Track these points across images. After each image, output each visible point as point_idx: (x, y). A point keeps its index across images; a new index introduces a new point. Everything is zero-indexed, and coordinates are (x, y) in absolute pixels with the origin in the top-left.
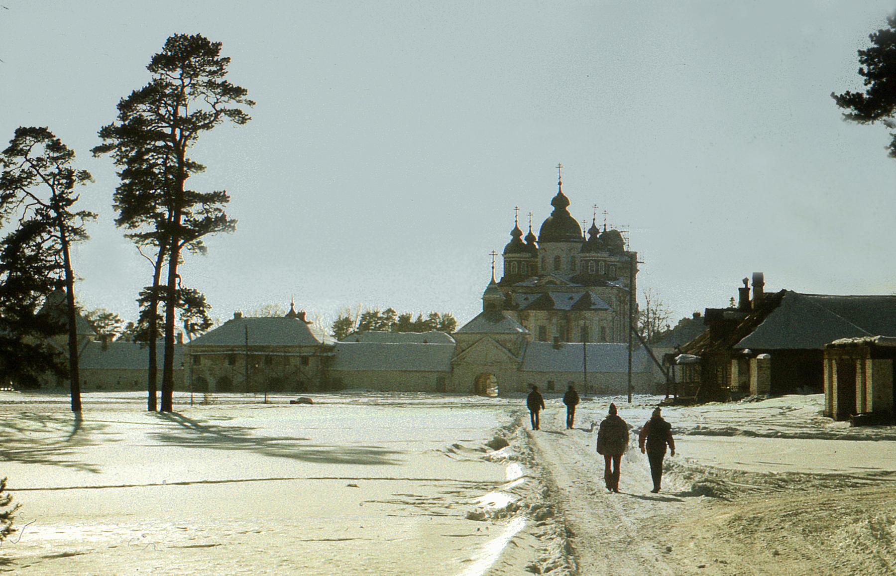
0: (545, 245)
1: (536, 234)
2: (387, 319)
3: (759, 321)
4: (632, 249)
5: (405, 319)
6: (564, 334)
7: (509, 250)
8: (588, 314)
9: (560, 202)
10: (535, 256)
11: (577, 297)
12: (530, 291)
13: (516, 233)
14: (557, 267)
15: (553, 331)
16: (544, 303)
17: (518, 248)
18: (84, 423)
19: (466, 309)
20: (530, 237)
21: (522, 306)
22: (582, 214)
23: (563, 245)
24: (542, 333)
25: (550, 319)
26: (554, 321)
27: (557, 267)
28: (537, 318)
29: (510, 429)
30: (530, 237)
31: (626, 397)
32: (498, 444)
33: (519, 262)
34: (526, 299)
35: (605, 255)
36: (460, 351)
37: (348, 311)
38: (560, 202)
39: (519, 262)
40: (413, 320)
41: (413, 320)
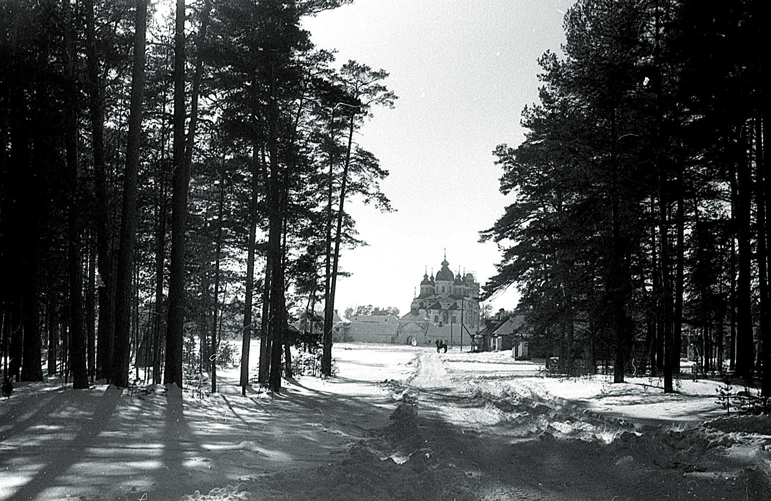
0: (438, 281)
1: (435, 276)
2: (369, 309)
3: (502, 324)
4: (478, 282)
6: (445, 320)
7: (422, 283)
8: (455, 311)
9: (445, 264)
10: (434, 286)
11: (451, 304)
12: (431, 301)
13: (426, 276)
14: (443, 291)
16: (437, 306)
17: (427, 282)
18: (337, 365)
19: (405, 309)
20: (432, 278)
21: (428, 308)
22: (454, 268)
23: (447, 282)
25: (439, 313)
26: (441, 314)
27: (443, 291)
28: (433, 313)
29: (415, 360)
30: (432, 278)
31: (460, 347)
32: (410, 363)
33: (427, 289)
35: (464, 286)
36: (401, 327)
37: (352, 305)
38: (445, 264)
40: (380, 310)
41: (380, 310)
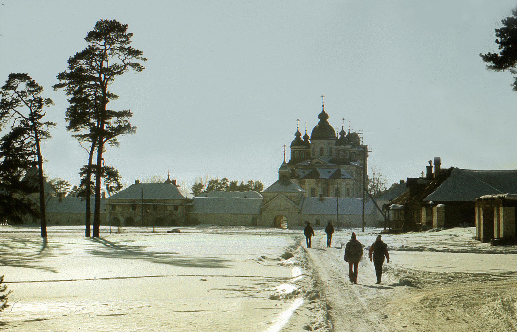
0: (315, 141)
1: (310, 135)
2: (223, 184)
3: (438, 185)
4: (364, 144)
5: (234, 184)
6: (326, 193)
7: (293, 144)
8: (339, 181)
9: (323, 116)
10: (309, 148)
11: (333, 171)
12: (306, 167)
13: (298, 134)
14: (321, 154)
16: (314, 175)
17: (299, 143)
19: (269, 178)
20: (306, 137)
21: (301, 176)
22: (336, 124)
23: (325, 141)
24: (313, 192)
25: (317, 184)
26: (320, 185)
27: (321, 154)
28: (310, 183)
29: (295, 247)
30: (306, 137)
31: (361, 229)
32: (287, 256)
33: (300, 151)
34: (304, 172)
35: (349, 147)
36: (265, 202)
37: (201, 179)
38: (323, 116)
40: (238, 184)
41: (238, 184)
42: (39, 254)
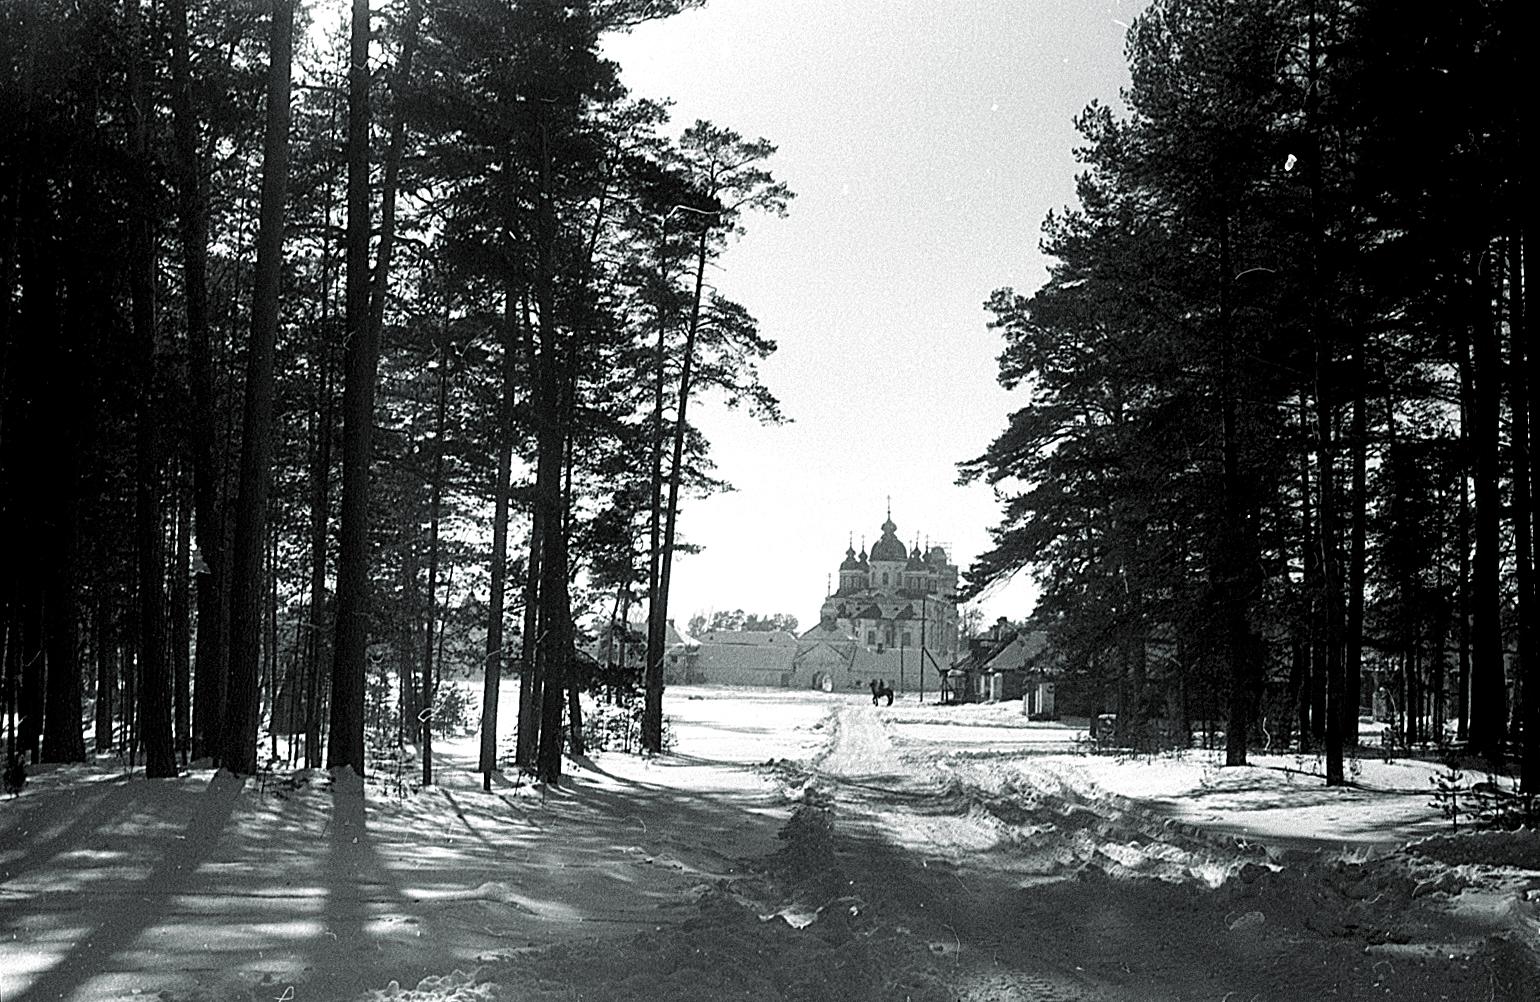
0: (874, 563)
1: (868, 552)
2: (738, 618)
3: (1003, 648)
4: (954, 563)
5: (752, 619)
6: (890, 640)
7: (843, 566)
8: (909, 623)
9: (889, 528)
10: (867, 572)
11: (901, 608)
12: (861, 602)
13: (851, 552)
14: (886, 582)
15: (880, 637)
16: (873, 613)
17: (852, 563)
19: (808, 619)
20: (863, 555)
21: (854, 615)
22: (906, 537)
23: (893, 564)
24: (871, 637)
25: (878, 626)
26: (882, 627)
27: (886, 582)
28: (865, 626)
29: (829, 719)
30: (863, 555)
31: (918, 694)
32: (819, 727)
33: (852, 577)
34: (858, 609)
35: (926, 572)
36: (801, 653)
37: (702, 611)
38: (889, 528)
39: (852, 577)
40: (759, 620)
41: (759, 620)
42: (1321, 788)
